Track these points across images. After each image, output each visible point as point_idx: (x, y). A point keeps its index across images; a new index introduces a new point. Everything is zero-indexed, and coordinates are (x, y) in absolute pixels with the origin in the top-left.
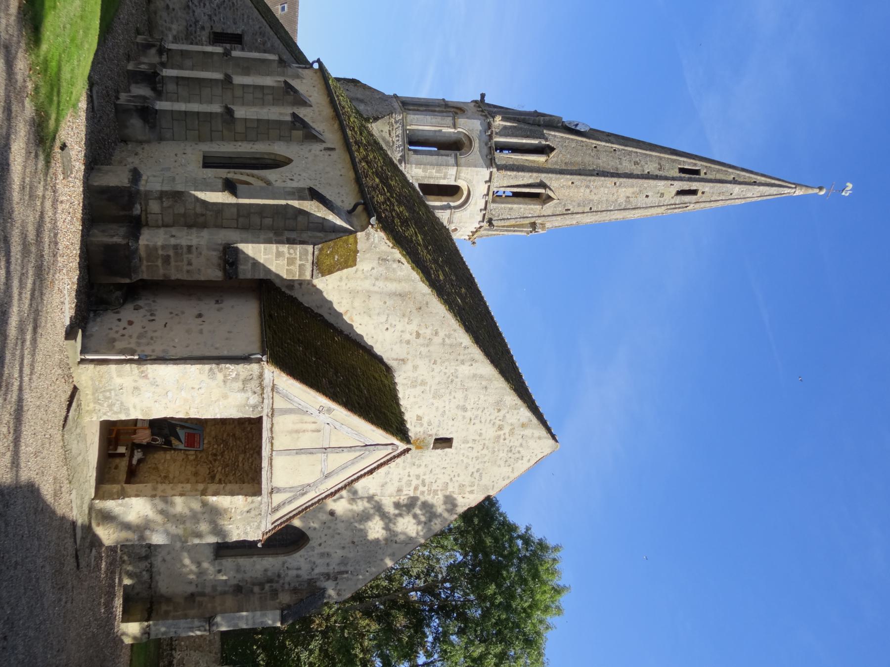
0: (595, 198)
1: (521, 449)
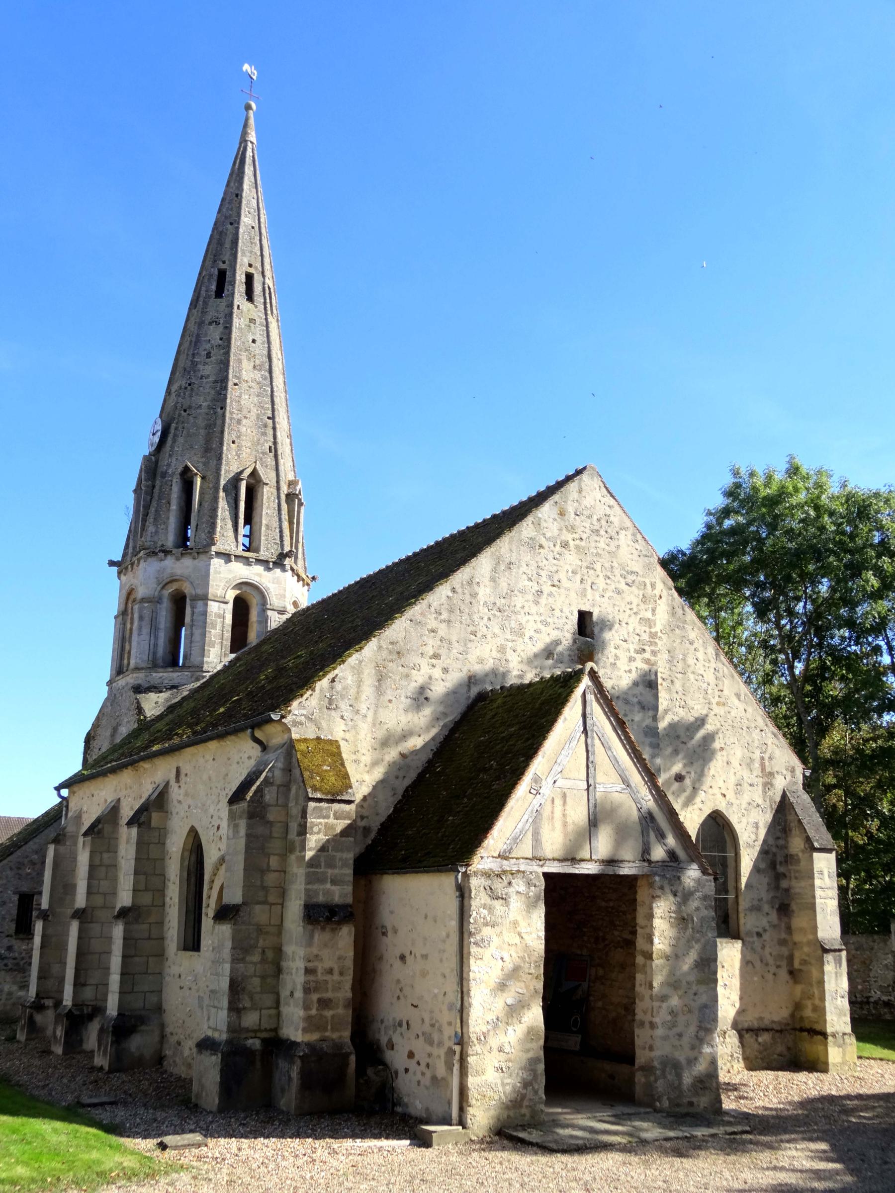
0: (254, 411)
1: (595, 517)
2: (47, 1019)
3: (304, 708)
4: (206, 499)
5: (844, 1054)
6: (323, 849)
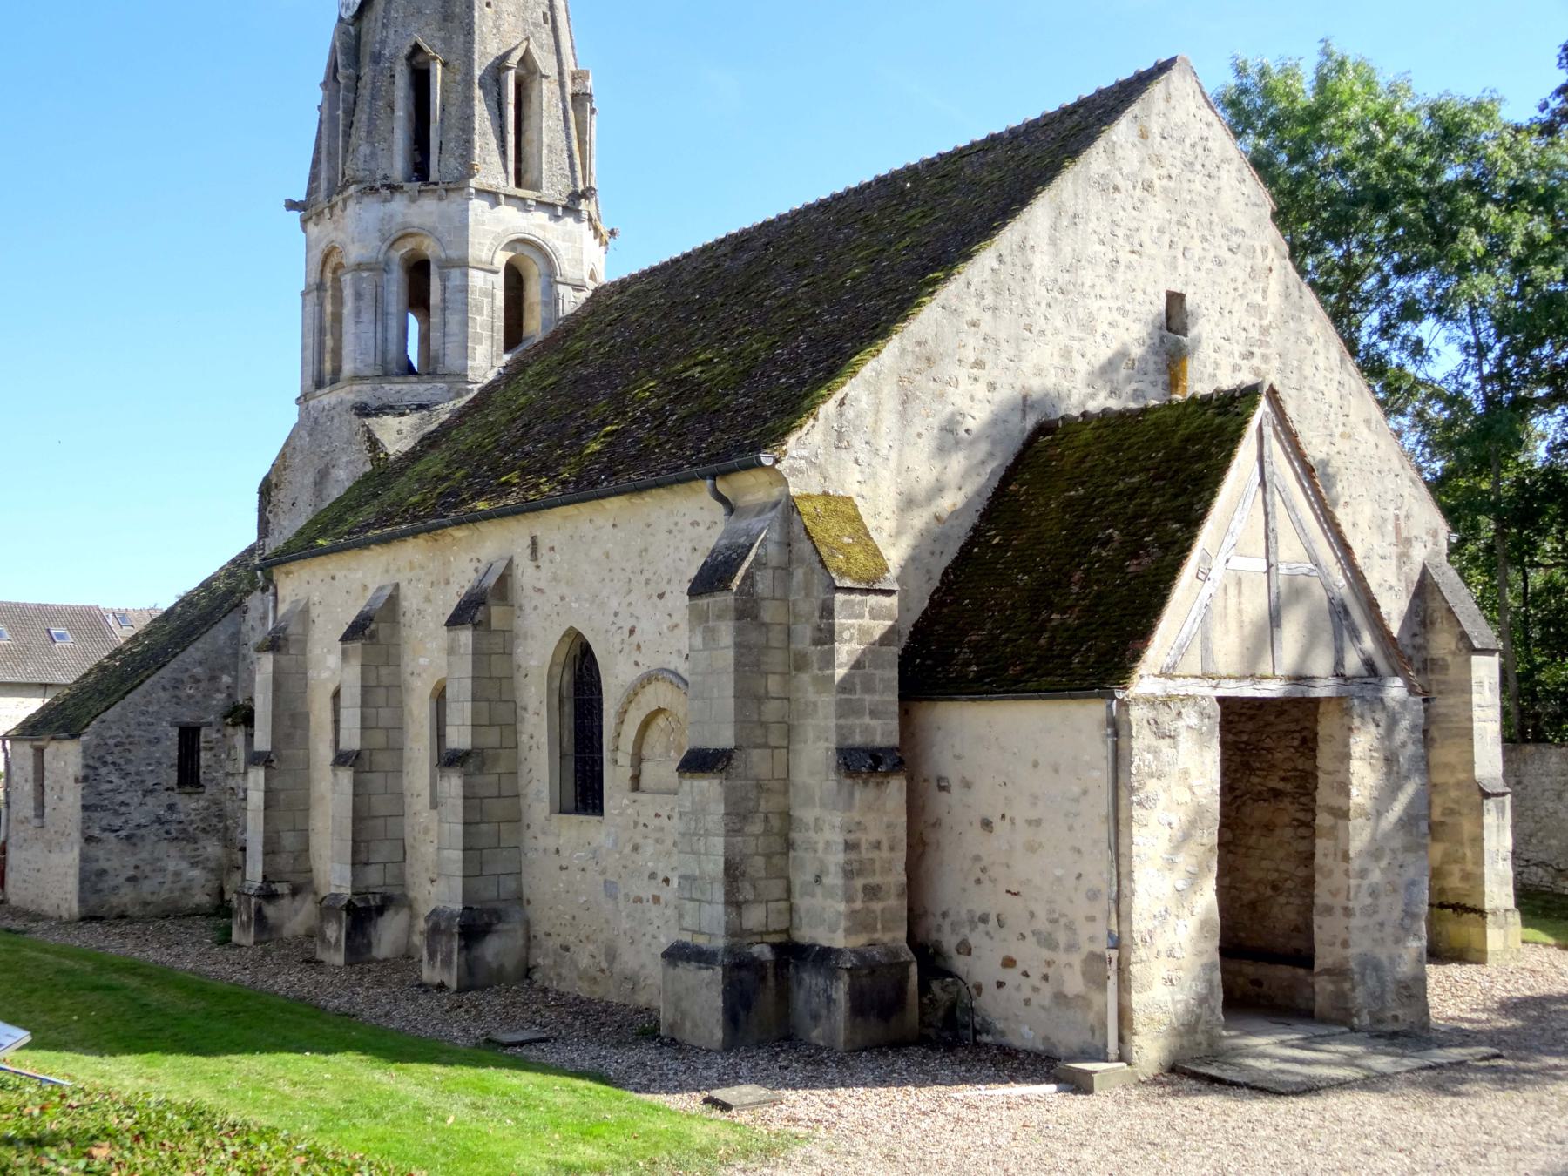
1: (1188, 142)
2: (295, 917)
3: (804, 446)
4: (452, 101)
5: (1506, 938)
6: (857, 665)
